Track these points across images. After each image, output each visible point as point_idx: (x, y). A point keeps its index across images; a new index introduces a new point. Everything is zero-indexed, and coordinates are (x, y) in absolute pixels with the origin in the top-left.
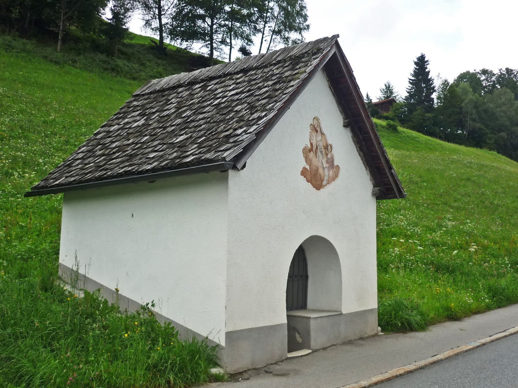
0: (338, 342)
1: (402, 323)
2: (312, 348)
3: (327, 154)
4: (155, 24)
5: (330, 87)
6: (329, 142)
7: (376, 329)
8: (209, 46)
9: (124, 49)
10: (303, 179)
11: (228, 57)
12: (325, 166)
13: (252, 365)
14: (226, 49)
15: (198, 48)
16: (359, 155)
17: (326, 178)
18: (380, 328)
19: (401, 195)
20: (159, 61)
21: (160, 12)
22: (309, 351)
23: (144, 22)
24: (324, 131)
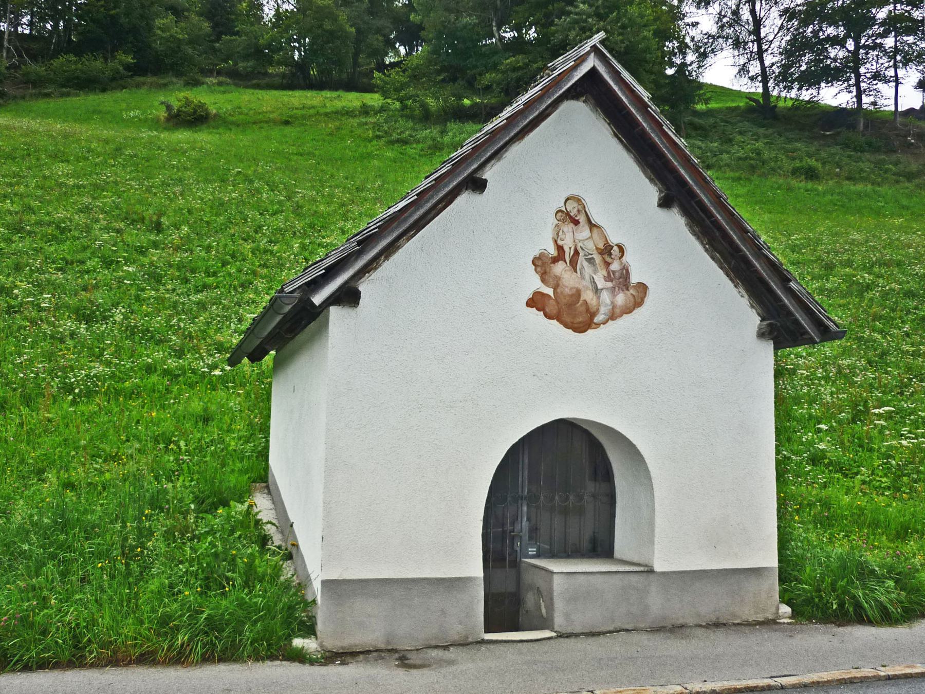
0: (642, 626)
1: (841, 605)
2: (556, 628)
3: (608, 264)
4: (755, 68)
5: (616, 135)
6: (614, 239)
7: (773, 610)
8: (854, 89)
9: (696, 120)
10: (536, 316)
11: (892, 101)
12: (600, 287)
13: (388, 643)
14: (887, 90)
15: (834, 96)
16: (713, 258)
17: (603, 310)
18: (785, 609)
19: (826, 333)
20: (762, 131)
21: (760, 47)
22: (554, 634)
23: (737, 69)
24: (596, 218)
